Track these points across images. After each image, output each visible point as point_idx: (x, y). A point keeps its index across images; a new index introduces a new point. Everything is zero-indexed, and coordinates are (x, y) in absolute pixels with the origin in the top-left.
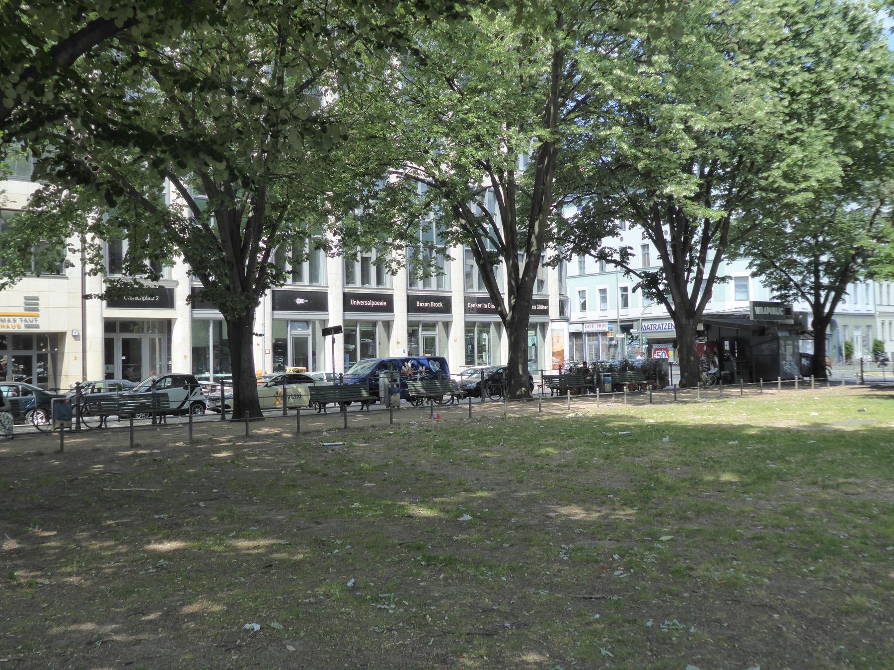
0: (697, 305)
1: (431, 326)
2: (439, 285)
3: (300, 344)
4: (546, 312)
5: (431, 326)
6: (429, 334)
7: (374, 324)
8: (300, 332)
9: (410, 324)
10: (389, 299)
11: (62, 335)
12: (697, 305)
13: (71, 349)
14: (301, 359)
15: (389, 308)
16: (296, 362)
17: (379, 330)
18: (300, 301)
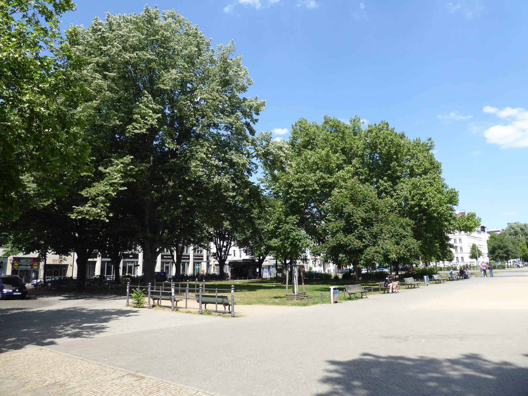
0: (9, 340)
1: (168, 263)
2: (187, 252)
3: (130, 267)
4: (203, 259)
5: (168, 263)
6: (167, 265)
7: (185, 262)
8: (130, 264)
9: (162, 262)
10: (189, 256)
11: (68, 265)
12: (9, 340)
13: (70, 268)
14: (130, 272)
15: (189, 259)
16: (129, 273)
17: (186, 264)
18: (131, 256)
